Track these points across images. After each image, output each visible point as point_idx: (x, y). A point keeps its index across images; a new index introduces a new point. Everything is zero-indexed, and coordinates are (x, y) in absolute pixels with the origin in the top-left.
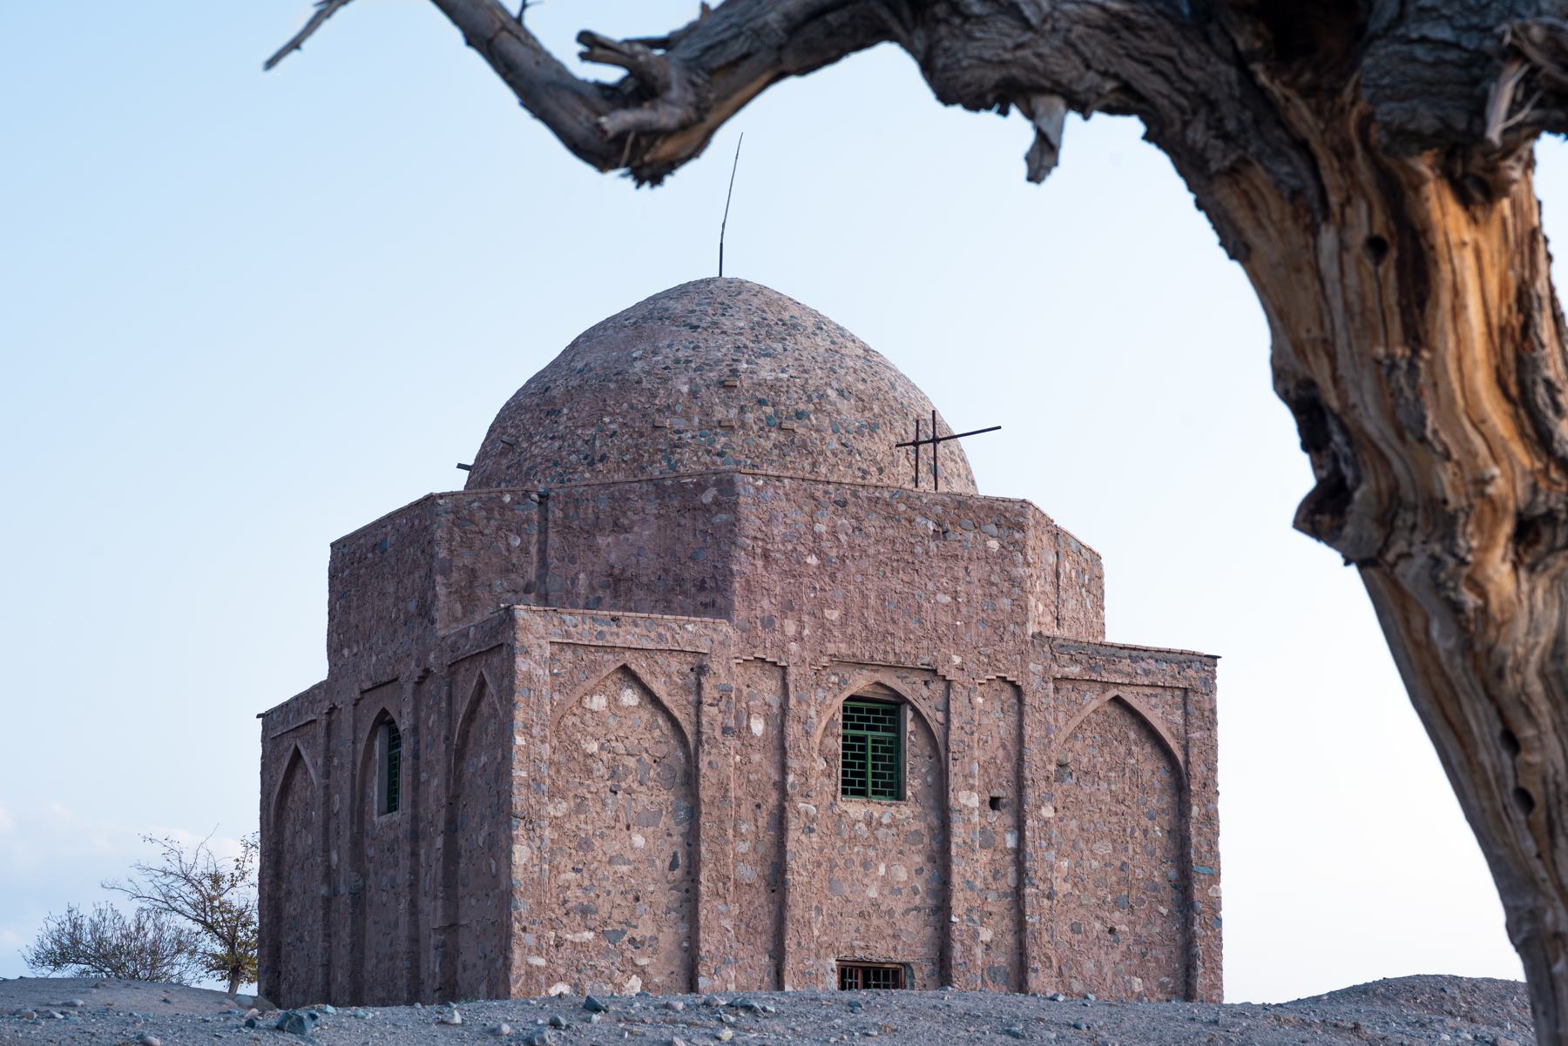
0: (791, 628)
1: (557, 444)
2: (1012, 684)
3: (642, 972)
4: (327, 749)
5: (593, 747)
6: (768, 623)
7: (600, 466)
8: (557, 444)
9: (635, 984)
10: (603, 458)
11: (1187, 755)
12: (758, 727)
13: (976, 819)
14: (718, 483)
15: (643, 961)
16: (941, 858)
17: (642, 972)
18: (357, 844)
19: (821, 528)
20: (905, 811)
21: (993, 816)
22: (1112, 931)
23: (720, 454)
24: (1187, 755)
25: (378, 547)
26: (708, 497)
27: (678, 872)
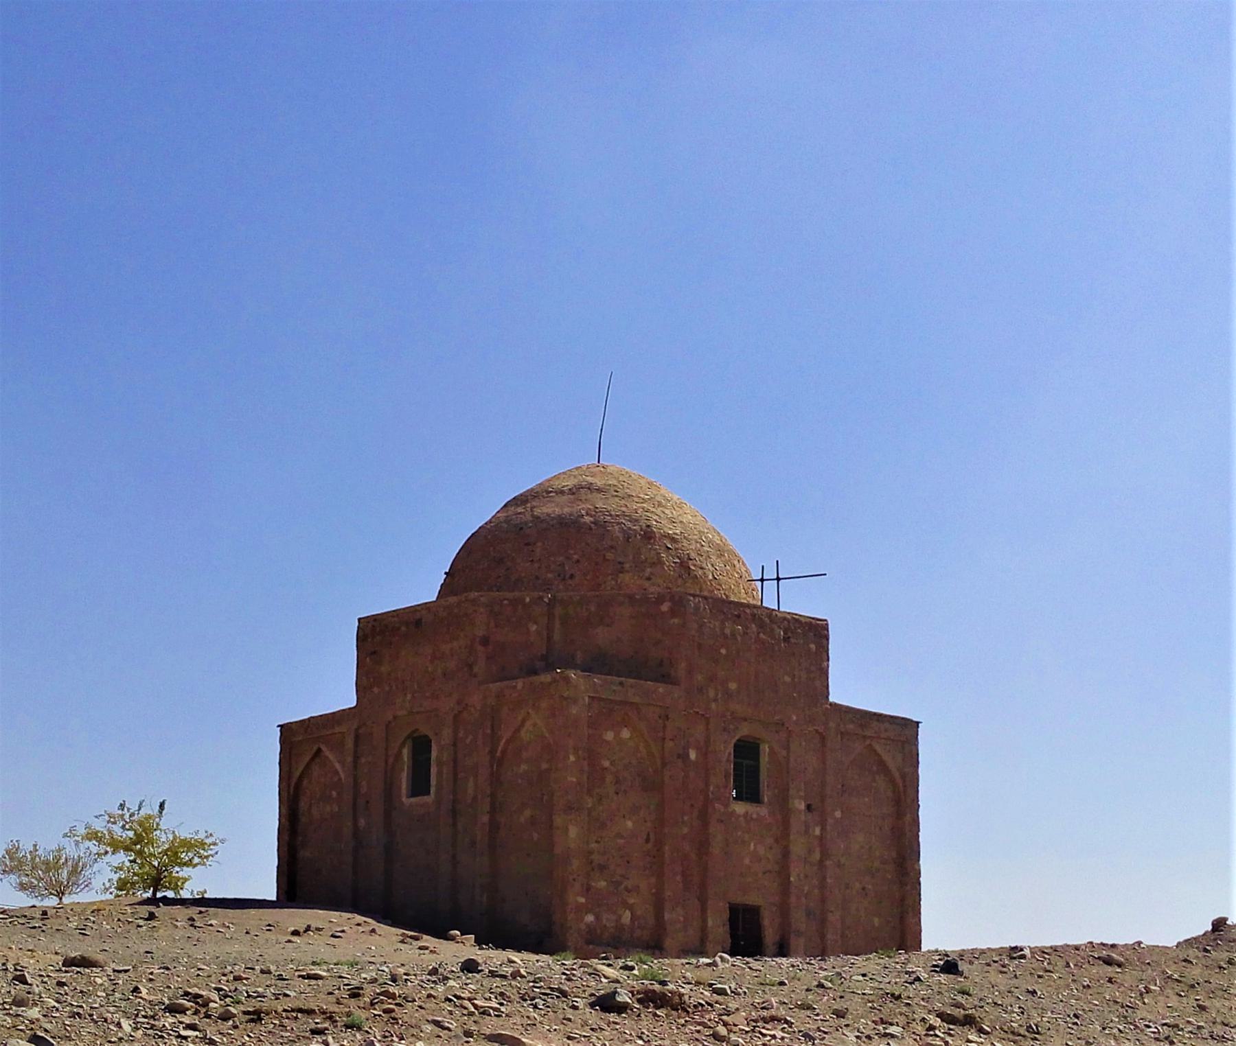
0: (712, 693)
1: (536, 565)
2: (821, 734)
3: (631, 908)
4: (355, 752)
5: (606, 764)
6: (700, 690)
7: (570, 582)
8: (536, 565)
9: (626, 917)
10: (572, 576)
11: (904, 781)
12: (693, 755)
13: (803, 818)
14: (672, 599)
15: (631, 901)
16: (783, 838)
17: (631, 908)
18: (388, 815)
19: (728, 631)
20: (763, 811)
21: (810, 816)
22: (864, 889)
23: (649, 579)
24: (904, 781)
25: (418, 623)
26: (665, 607)
27: (650, 846)
